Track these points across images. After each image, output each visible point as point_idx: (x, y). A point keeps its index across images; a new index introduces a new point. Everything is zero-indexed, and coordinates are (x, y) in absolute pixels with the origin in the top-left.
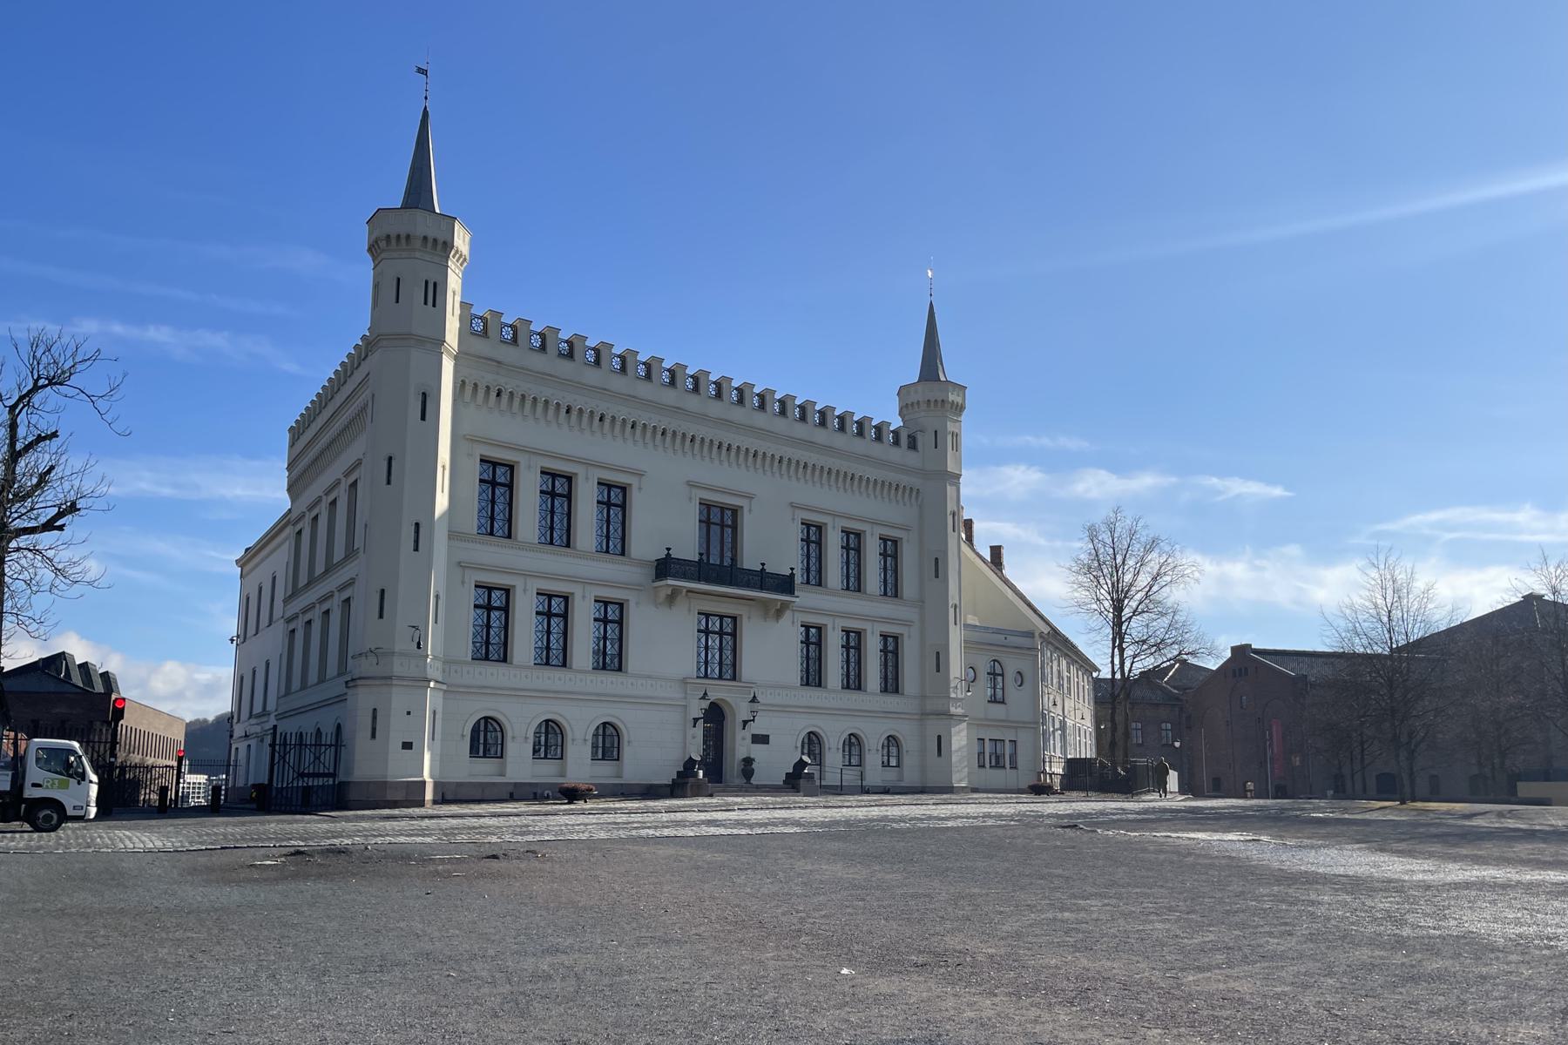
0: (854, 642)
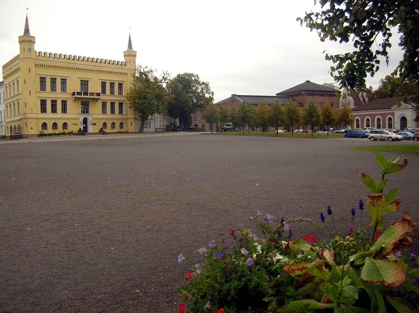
0: (113, 104)
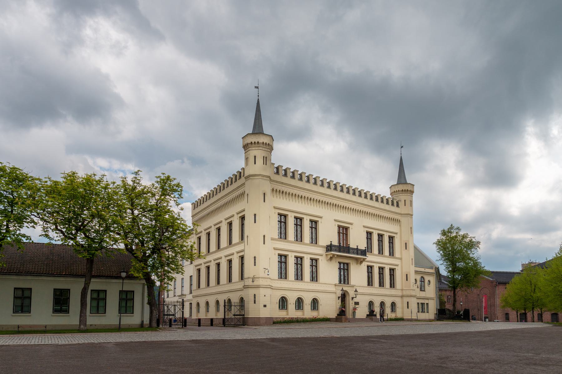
0: (299, 261)
